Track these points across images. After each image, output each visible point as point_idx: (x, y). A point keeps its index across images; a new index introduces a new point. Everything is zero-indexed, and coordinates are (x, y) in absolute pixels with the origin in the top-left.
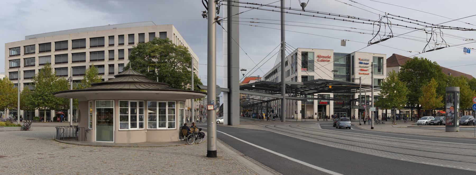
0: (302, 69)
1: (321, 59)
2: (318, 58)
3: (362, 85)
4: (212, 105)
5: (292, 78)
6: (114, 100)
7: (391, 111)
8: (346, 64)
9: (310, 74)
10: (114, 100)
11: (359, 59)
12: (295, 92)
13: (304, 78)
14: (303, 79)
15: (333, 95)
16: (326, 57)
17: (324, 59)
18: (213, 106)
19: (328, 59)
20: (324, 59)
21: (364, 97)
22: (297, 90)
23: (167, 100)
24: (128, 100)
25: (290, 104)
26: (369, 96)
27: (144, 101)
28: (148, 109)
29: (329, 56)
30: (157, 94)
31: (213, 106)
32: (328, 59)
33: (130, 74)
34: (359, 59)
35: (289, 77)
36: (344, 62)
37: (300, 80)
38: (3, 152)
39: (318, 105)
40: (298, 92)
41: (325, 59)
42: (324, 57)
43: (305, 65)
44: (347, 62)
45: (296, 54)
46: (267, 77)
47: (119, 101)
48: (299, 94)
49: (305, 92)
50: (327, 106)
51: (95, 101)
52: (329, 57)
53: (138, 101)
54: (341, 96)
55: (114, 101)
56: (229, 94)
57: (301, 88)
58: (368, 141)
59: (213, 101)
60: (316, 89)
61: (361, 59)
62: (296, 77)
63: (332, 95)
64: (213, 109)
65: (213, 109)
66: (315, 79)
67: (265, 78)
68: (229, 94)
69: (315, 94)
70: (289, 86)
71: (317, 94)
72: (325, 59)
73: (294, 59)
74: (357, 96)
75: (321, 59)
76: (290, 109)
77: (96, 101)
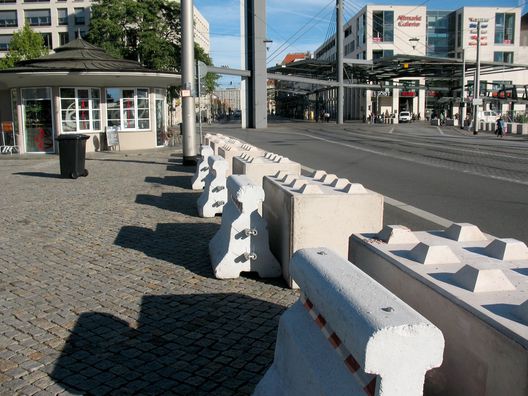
0: (373, 39)
1: (406, 22)
2: (399, 21)
3: (482, 65)
4: (188, 90)
5: (358, 53)
6: (52, 86)
7: (526, 107)
8: (448, 28)
9: (385, 46)
10: (52, 86)
11: (471, 20)
12: (360, 76)
13: (377, 54)
14: (376, 55)
15: (425, 80)
16: (413, 19)
17: (410, 22)
18: (189, 91)
19: (417, 22)
20: (410, 22)
21: (472, 83)
22: (363, 72)
23: (135, 87)
24: (73, 87)
25: (355, 96)
26: (486, 81)
27: (100, 88)
28: (106, 101)
29: (419, 17)
30: (118, 76)
31: (189, 91)
32: (417, 22)
33: (77, 46)
34: (471, 20)
35: (353, 52)
36: (445, 26)
37: (370, 56)
38: (17, 267)
39: (399, 98)
40: (365, 77)
41: (413, 22)
42: (409, 18)
43: (378, 30)
44: (449, 25)
45: (365, 17)
46: (319, 54)
47: (60, 88)
48: (368, 79)
49: (377, 76)
50: (415, 100)
51: (21, 89)
52: (419, 19)
53: (91, 88)
54: (438, 82)
55: (51, 88)
56: (250, 81)
57: (370, 69)
58: (476, 153)
59: (190, 83)
60: (394, 71)
61: (473, 19)
62: (365, 53)
63: (422, 81)
64: (189, 95)
65: (189, 95)
66: (395, 53)
67: (317, 54)
68: (250, 81)
69: (395, 80)
70: (349, 67)
71: (397, 80)
72: (413, 22)
73: (389, 26)
74: (466, 80)
75: (406, 22)
76: (355, 104)
77: (22, 90)
